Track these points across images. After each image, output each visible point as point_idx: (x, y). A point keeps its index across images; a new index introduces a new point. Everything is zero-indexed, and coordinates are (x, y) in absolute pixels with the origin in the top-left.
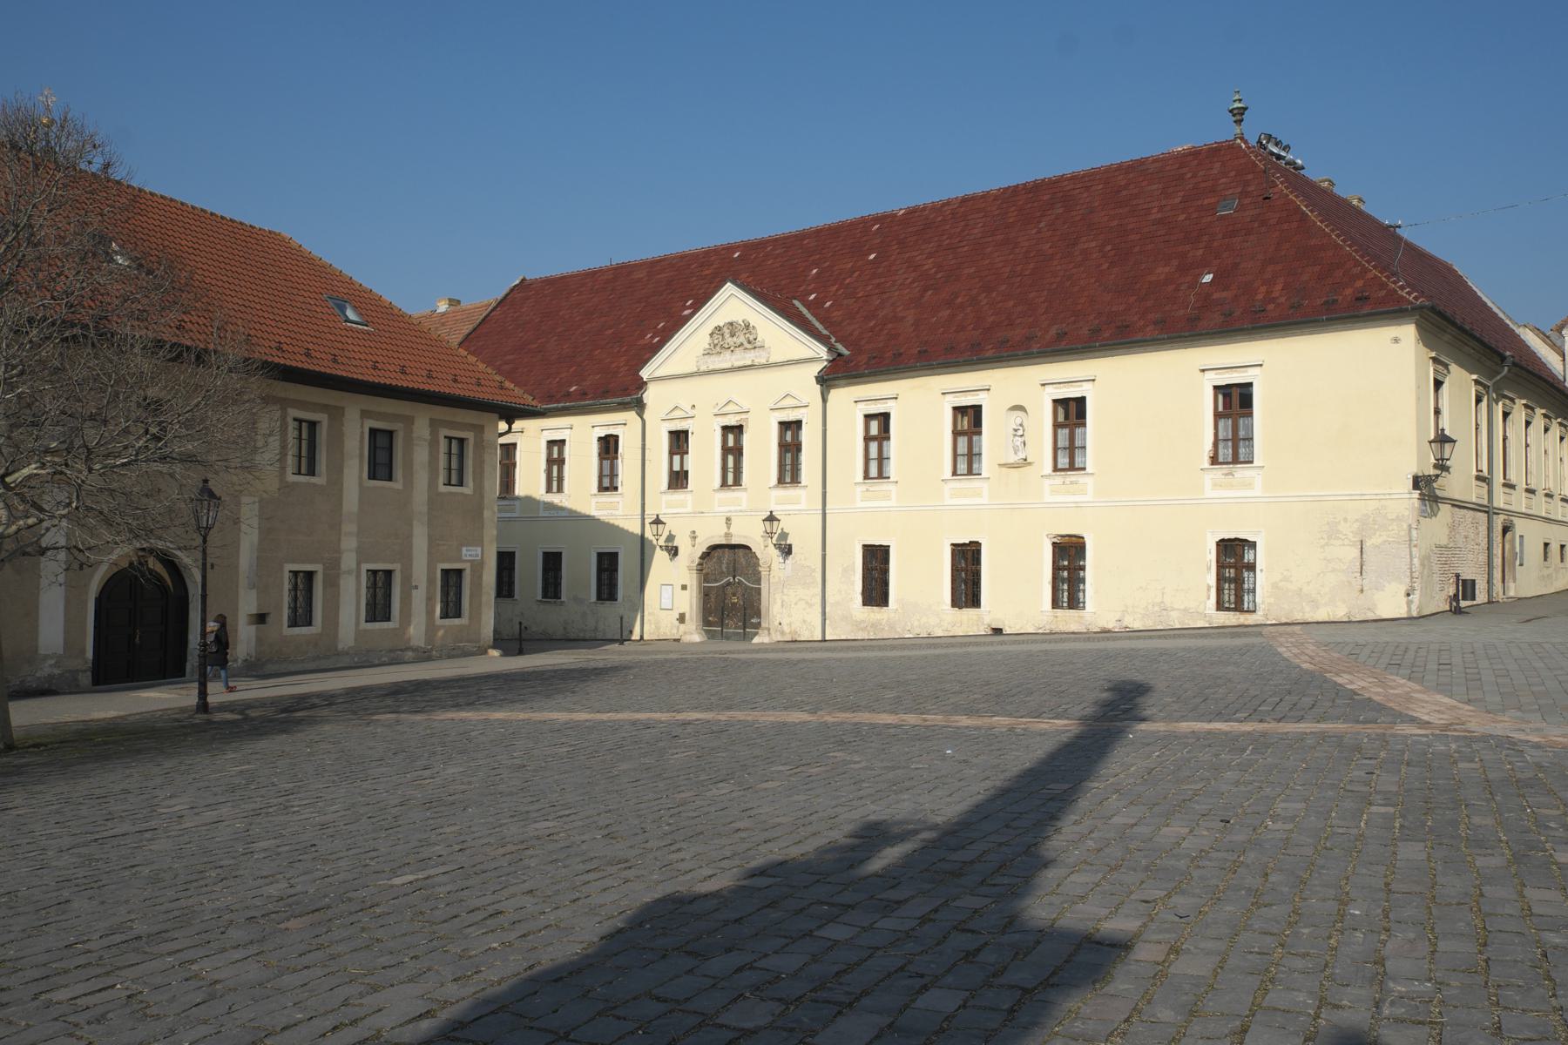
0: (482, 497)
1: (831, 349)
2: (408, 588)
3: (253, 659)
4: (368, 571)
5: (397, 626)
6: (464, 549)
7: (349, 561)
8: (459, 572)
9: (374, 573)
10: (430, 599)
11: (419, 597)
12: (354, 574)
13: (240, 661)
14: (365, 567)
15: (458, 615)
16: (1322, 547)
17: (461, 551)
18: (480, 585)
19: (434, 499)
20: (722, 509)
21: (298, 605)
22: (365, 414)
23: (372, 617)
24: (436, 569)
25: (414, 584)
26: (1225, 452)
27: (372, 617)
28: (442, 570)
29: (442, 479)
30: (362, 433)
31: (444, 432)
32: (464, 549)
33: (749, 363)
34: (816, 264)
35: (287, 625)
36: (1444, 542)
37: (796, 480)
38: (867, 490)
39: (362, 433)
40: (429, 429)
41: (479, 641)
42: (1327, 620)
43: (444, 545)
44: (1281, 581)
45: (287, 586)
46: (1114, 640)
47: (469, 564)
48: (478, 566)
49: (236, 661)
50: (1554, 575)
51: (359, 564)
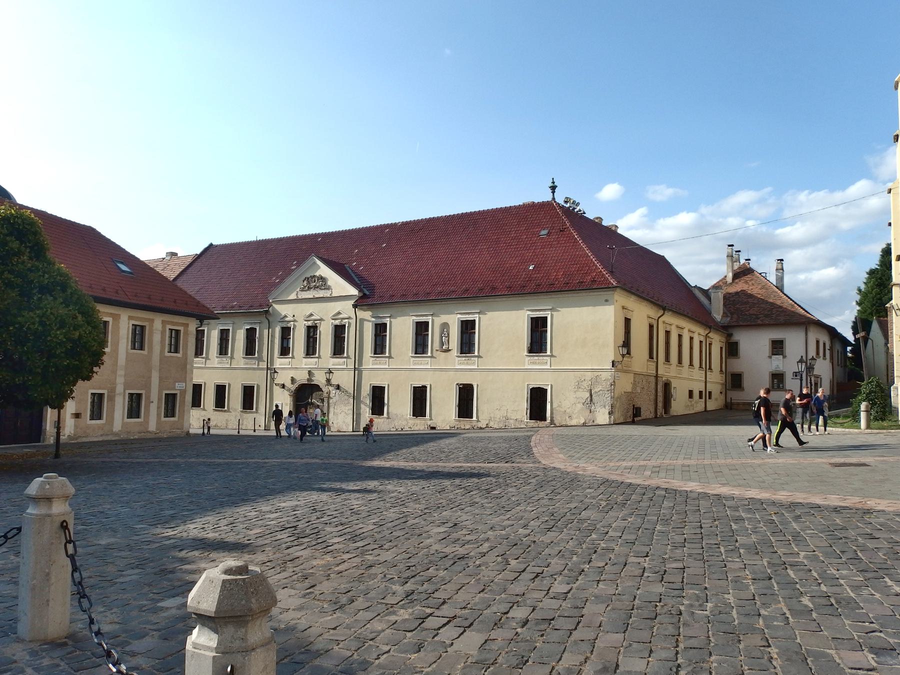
0: (186, 359)
1: (360, 291)
2: (149, 402)
3: (72, 435)
4: (129, 393)
5: (143, 421)
6: (177, 384)
7: (120, 388)
8: (174, 395)
9: (131, 395)
10: (159, 408)
11: (153, 408)
12: (123, 395)
13: (66, 436)
14: (128, 391)
15: (173, 416)
16: (575, 392)
17: (175, 385)
18: (184, 401)
19: (162, 358)
20: (306, 367)
21: (95, 410)
22: (130, 318)
23: (130, 416)
24: (88, 393)
25: (151, 400)
26: (420, 350)
27: (130, 416)
28: (166, 394)
29: (167, 349)
30: (129, 327)
31: (169, 327)
32: (177, 384)
33: (322, 296)
34: (357, 247)
35: (89, 419)
36: (630, 390)
37: (424, 351)
38: (375, 360)
39: (129, 327)
40: (161, 325)
41: (183, 429)
42: (576, 424)
43: (167, 382)
44: (557, 407)
45: (89, 400)
46: (158, 415)
47: (179, 391)
48: (184, 392)
49: (64, 436)
50: (695, 405)
51: (124, 391)
